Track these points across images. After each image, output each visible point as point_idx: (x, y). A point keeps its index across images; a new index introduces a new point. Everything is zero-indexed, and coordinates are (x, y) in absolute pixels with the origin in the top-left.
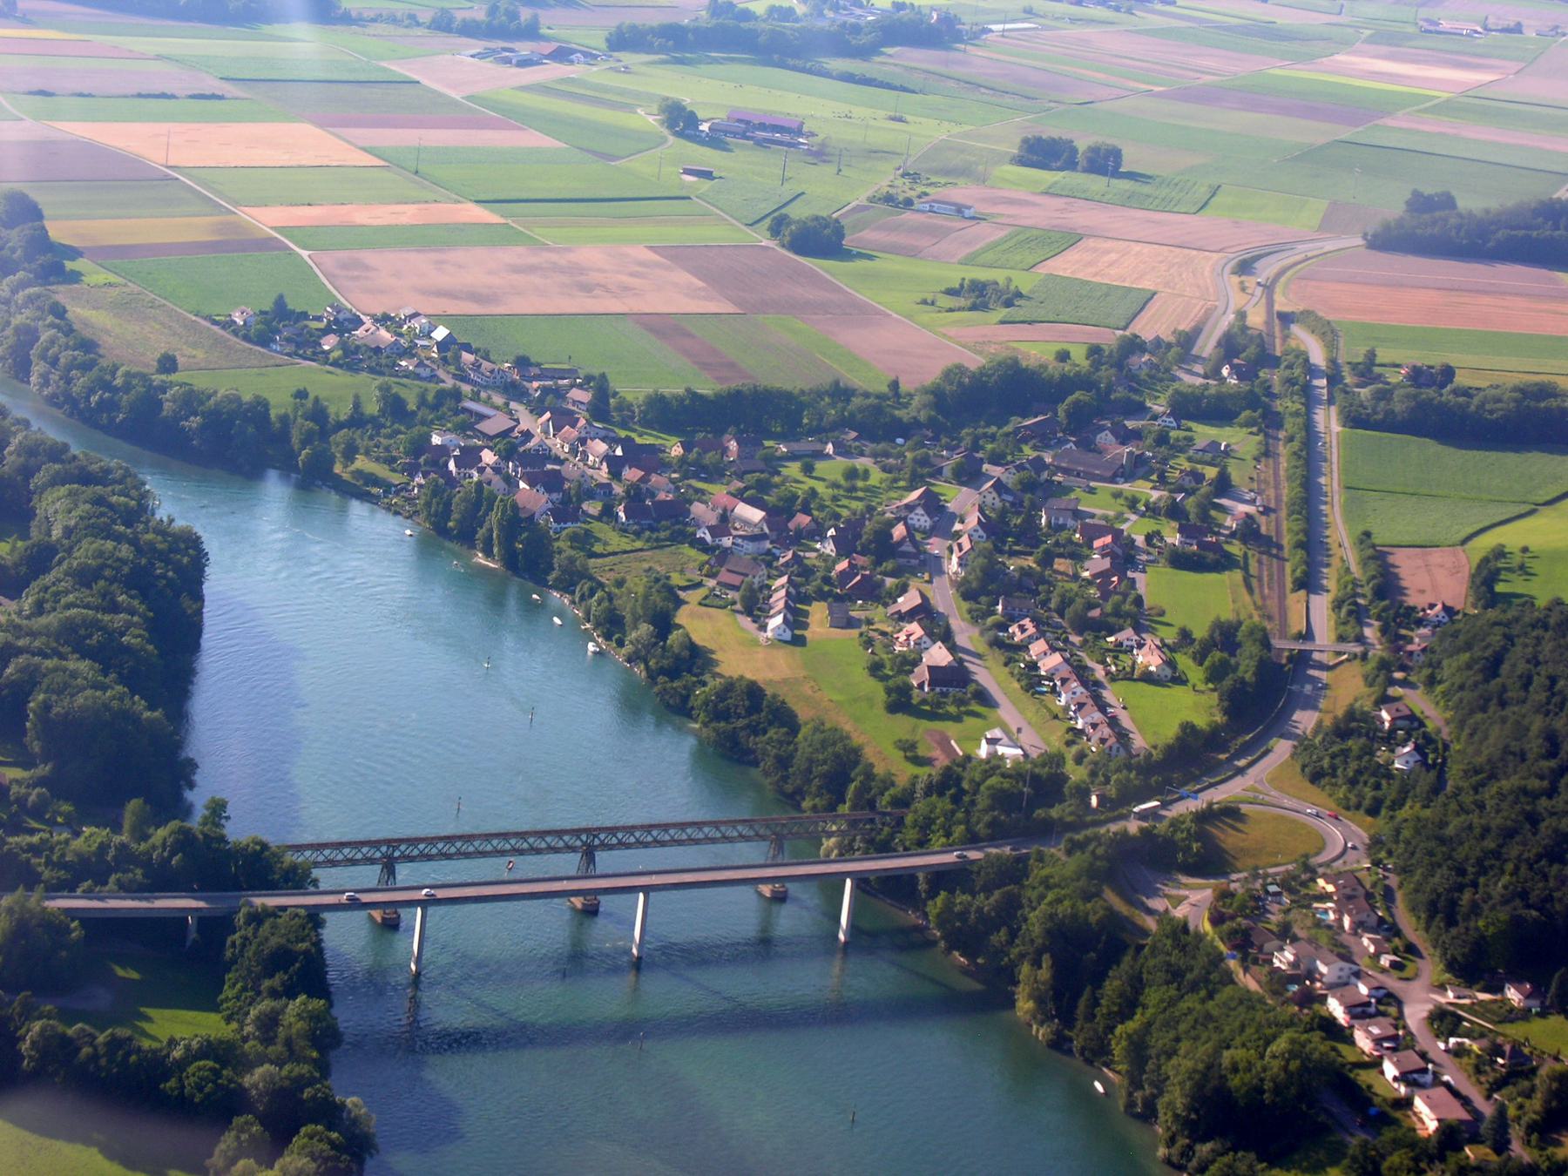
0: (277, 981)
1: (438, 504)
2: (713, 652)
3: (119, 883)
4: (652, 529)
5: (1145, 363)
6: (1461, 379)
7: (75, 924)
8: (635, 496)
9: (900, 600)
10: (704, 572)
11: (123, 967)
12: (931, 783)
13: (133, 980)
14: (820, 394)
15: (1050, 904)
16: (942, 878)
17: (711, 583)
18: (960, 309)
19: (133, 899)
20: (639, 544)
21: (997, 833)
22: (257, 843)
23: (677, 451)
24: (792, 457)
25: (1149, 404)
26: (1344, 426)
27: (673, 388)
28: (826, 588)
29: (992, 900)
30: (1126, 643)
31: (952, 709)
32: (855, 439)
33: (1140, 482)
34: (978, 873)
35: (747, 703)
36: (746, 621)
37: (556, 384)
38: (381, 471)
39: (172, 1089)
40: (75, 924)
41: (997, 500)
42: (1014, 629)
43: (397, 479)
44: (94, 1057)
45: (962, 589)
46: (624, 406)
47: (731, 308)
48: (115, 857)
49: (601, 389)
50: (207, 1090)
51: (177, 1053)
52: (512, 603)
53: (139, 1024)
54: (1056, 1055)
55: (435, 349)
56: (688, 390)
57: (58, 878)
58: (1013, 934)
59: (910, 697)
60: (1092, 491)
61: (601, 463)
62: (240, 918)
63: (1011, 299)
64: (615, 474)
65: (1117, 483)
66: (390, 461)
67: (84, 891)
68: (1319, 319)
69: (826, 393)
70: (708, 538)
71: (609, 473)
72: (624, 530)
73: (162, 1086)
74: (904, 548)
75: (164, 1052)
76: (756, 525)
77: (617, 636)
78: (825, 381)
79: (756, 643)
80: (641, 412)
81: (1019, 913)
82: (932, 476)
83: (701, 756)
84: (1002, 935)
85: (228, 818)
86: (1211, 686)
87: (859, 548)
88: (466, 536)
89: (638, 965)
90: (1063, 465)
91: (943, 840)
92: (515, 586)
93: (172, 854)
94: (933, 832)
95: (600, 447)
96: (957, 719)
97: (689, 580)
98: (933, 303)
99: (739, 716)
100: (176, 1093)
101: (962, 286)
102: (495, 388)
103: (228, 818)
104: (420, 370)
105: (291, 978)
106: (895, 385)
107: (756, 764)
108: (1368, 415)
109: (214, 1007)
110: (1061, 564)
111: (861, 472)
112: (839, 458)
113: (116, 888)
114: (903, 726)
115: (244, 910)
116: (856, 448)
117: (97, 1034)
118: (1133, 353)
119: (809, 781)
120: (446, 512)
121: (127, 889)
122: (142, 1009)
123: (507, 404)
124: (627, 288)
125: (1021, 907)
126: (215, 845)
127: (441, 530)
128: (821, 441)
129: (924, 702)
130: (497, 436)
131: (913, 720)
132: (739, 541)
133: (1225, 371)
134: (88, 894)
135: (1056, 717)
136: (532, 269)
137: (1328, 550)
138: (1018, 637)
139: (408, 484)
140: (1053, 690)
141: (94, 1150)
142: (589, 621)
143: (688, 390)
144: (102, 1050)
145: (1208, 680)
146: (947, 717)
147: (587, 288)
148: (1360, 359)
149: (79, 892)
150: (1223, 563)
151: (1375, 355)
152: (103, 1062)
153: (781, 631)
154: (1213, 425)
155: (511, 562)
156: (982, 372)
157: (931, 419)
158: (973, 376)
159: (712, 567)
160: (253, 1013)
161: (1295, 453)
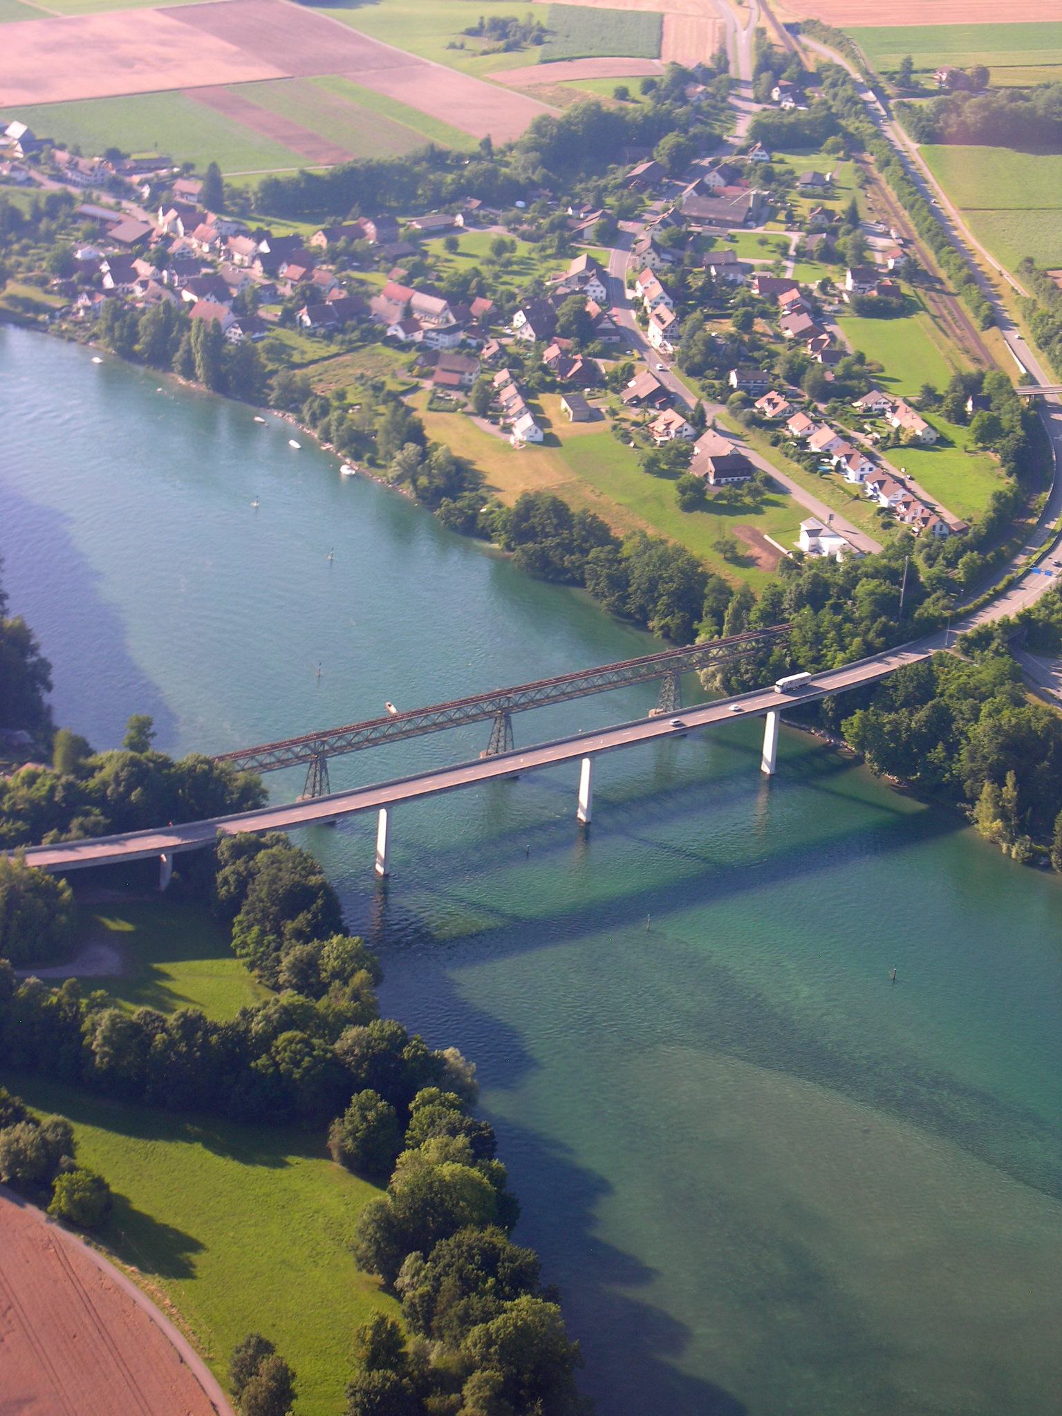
0: (302, 919)
1: (122, 328)
2: (472, 463)
3: (82, 827)
4: (343, 331)
5: (701, 93)
6: (995, 80)
7: (63, 883)
8: (311, 296)
9: (631, 384)
10: (415, 372)
11: (113, 920)
12: (801, 593)
13: (129, 932)
14: (417, 162)
15: (990, 715)
16: (850, 699)
17: (428, 384)
18: (495, 51)
19: (103, 843)
20: (334, 349)
21: (892, 642)
22: (201, 762)
23: (319, 240)
24: (430, 233)
25: (725, 137)
26: (919, 142)
27: (287, 171)
28: (548, 379)
29: (917, 717)
30: (875, 407)
31: (748, 500)
32: (479, 208)
33: (770, 224)
34: (895, 688)
35: (555, 521)
36: (484, 424)
37: (157, 176)
38: (36, 294)
39: (266, 1067)
40: (63, 883)
41: (657, 260)
42: (761, 403)
43: (58, 302)
44: (171, 1044)
45: (685, 366)
46: (237, 194)
47: (279, 74)
48: (65, 799)
49: (214, 180)
50: (305, 1064)
51: (257, 1026)
52: (224, 429)
53: (160, 983)
54: (1031, 870)
55: (19, 148)
56: (302, 172)
57: (17, 830)
58: (952, 749)
59: (704, 493)
60: (732, 239)
61: (253, 262)
62: (223, 850)
63: (539, 36)
64: (271, 271)
65: (750, 228)
66: (42, 282)
67: (52, 842)
68: (827, 29)
69: (423, 159)
70: (401, 334)
71: (265, 271)
72: (312, 335)
73: (253, 1065)
74: (603, 326)
75: (242, 1028)
76: (438, 316)
77: (368, 455)
78: (420, 147)
79: (509, 448)
80: (257, 199)
81: (954, 727)
82: (574, 239)
83: (502, 578)
84: (939, 752)
85: (153, 735)
86: (980, 445)
87: (559, 331)
88: (160, 356)
89: (587, 831)
90: (695, 214)
91: (840, 656)
92: (225, 409)
93: (129, 789)
94: (826, 646)
95: (247, 244)
96: (757, 510)
97: (403, 384)
98: (462, 47)
99: (547, 536)
100: (271, 1070)
101: (481, 25)
102: (101, 186)
103: (153, 735)
104: (15, 174)
105: (315, 916)
106: (487, 143)
107: (581, 583)
108: (941, 128)
109: (231, 954)
110: (760, 325)
111: (509, 244)
112: (472, 230)
113: (80, 833)
114: (704, 521)
115: (225, 843)
116: (484, 217)
117: (165, 1016)
118: (686, 83)
119: (655, 601)
120: (134, 337)
121: (94, 834)
122: (156, 966)
123: (119, 203)
124: (165, 60)
125: (953, 720)
126: (165, 771)
127: (126, 354)
128: (447, 213)
129: (720, 496)
130: (136, 242)
131: (714, 518)
132: (433, 335)
133: (776, 94)
134: (56, 845)
135: (857, 498)
136: (59, 47)
137: (989, 279)
138: (770, 413)
139: (70, 306)
140: (838, 468)
141: (198, 1146)
142: (329, 440)
143: (302, 172)
144: (177, 1035)
145: (978, 440)
146: (745, 510)
147: (127, 63)
148: (898, 68)
149: (46, 842)
150: (906, 308)
151: (911, 64)
152: (183, 1048)
153: (532, 433)
154: (798, 154)
155: (220, 384)
156: (568, 121)
157: (545, 178)
158: (560, 126)
159: (422, 367)
160: (286, 962)
161: (902, 179)
